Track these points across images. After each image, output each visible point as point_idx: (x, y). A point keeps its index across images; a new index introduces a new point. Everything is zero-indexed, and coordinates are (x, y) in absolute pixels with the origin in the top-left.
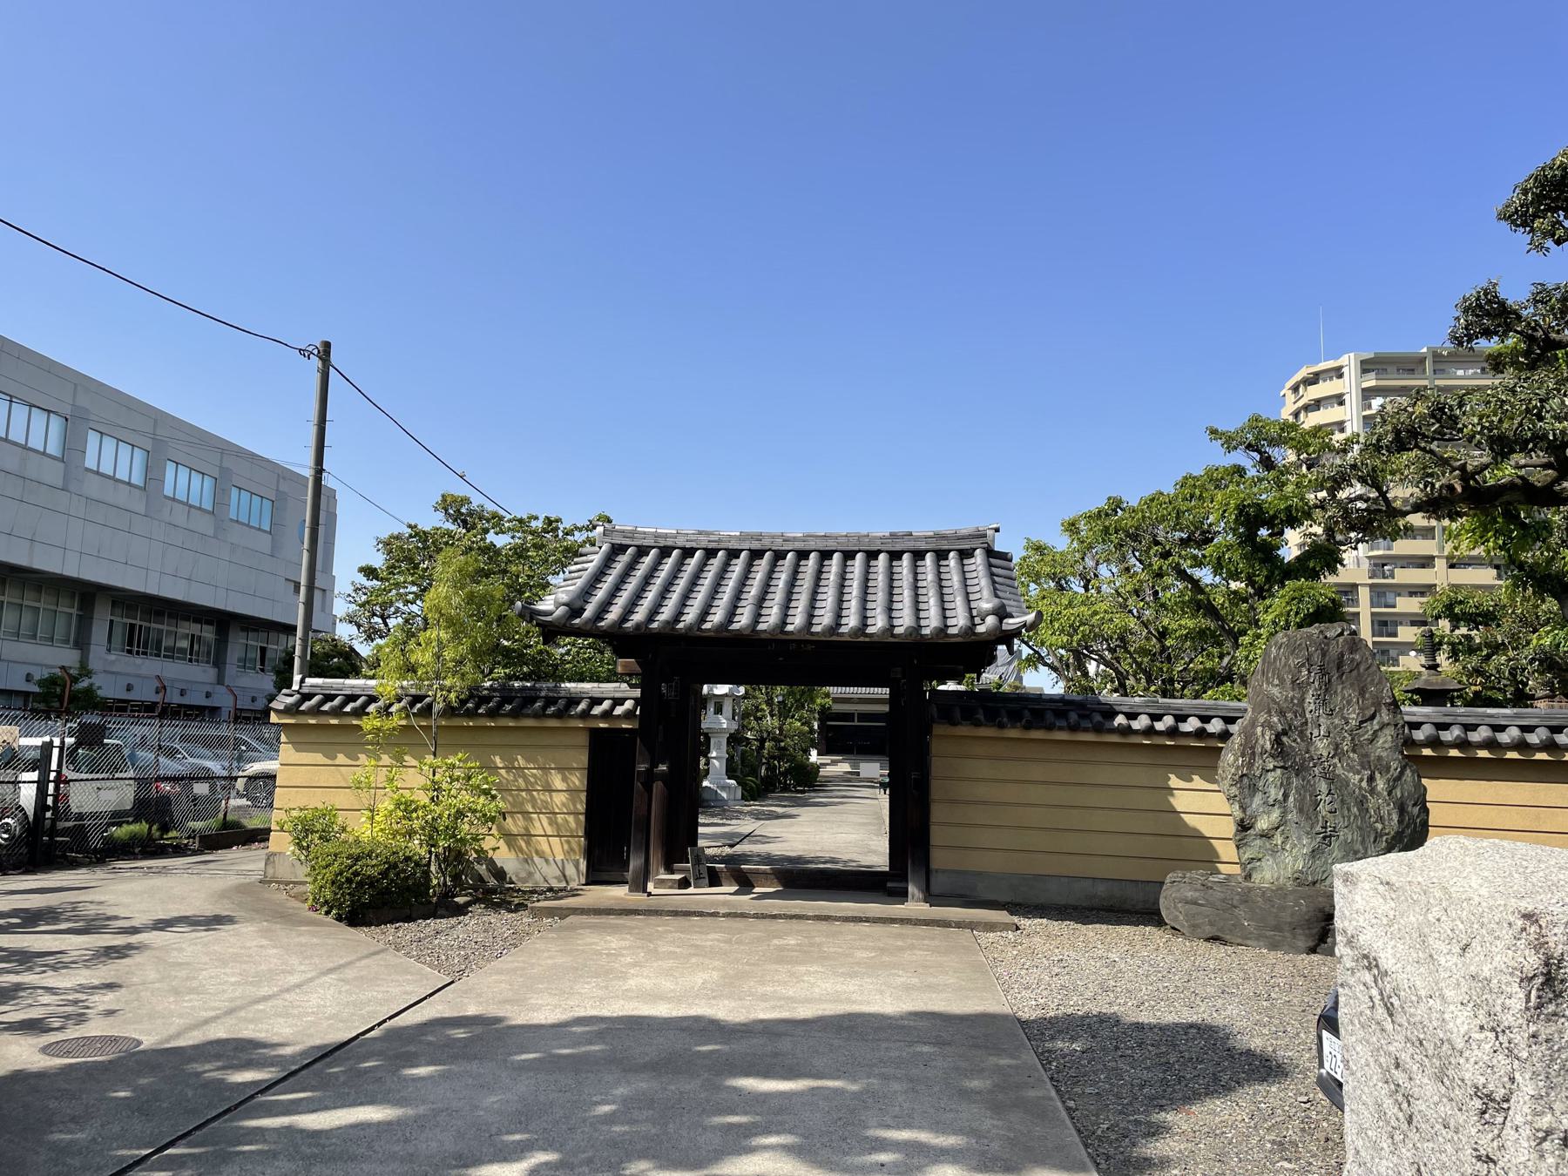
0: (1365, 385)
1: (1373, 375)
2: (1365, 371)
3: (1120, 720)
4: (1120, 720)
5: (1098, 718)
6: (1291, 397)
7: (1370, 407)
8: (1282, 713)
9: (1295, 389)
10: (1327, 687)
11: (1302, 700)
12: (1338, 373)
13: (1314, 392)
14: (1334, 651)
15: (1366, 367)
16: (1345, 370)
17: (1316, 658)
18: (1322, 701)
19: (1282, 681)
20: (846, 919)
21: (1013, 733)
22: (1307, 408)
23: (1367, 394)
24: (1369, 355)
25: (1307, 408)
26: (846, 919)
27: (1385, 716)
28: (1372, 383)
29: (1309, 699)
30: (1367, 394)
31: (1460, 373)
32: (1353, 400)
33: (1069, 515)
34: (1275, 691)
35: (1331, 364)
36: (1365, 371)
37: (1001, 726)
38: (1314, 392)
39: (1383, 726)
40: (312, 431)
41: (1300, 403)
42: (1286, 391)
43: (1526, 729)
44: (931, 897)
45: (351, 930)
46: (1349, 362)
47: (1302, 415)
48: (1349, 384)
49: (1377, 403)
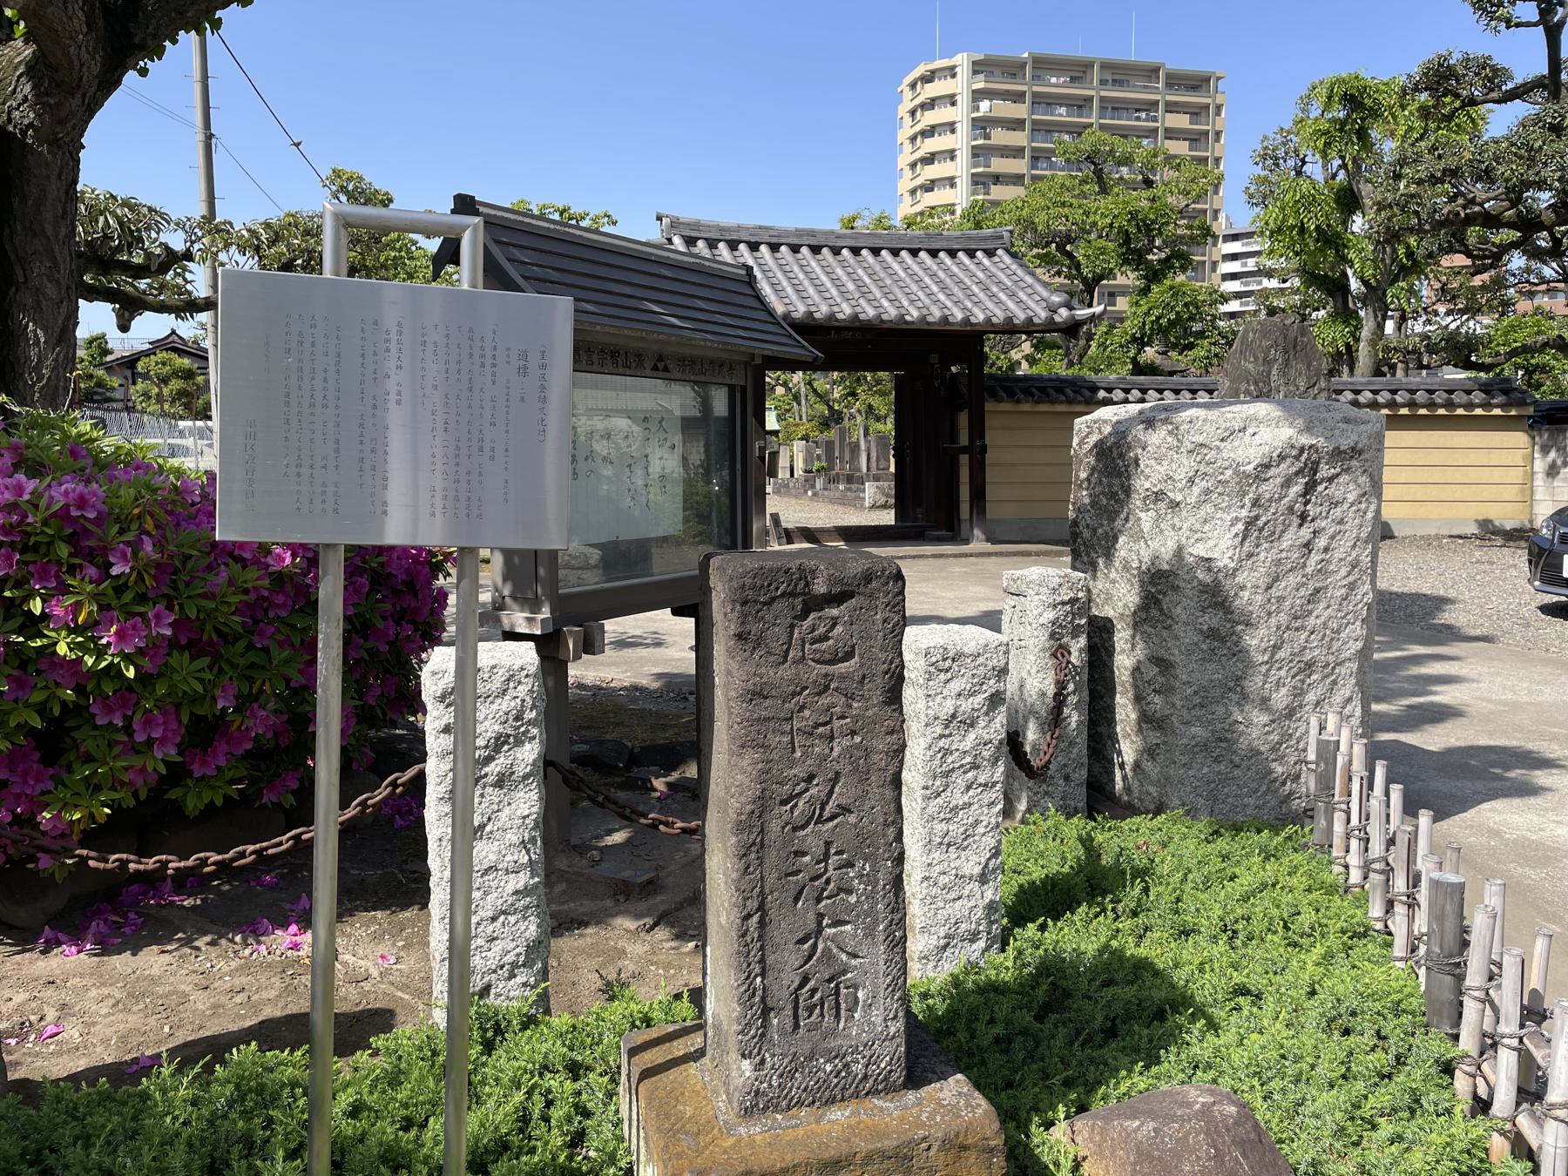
0: (975, 87)
1: (981, 77)
2: (975, 72)
3: (1102, 394)
4: (1102, 394)
5: (1088, 394)
6: (908, 94)
7: (978, 109)
8: (1256, 383)
9: (913, 86)
10: (1287, 363)
11: (1269, 373)
12: (951, 72)
13: (931, 90)
14: (1292, 335)
15: (978, 68)
16: (958, 70)
17: (1280, 341)
18: (1283, 372)
19: (1256, 358)
20: (914, 557)
21: (1025, 407)
22: (924, 106)
23: (977, 95)
24: (980, 56)
25: (924, 106)
26: (914, 557)
27: (1323, 384)
28: (981, 85)
29: (1274, 372)
30: (977, 95)
31: (1054, 80)
32: (963, 100)
33: (663, 211)
34: (1251, 366)
35: (945, 63)
36: (975, 72)
37: (1018, 402)
38: (931, 90)
39: (1321, 390)
40: (197, 88)
41: (918, 101)
42: (904, 87)
43: (1375, 392)
44: (990, 539)
45: (1491, 517)
46: (962, 61)
47: (918, 113)
48: (961, 85)
49: (985, 105)
